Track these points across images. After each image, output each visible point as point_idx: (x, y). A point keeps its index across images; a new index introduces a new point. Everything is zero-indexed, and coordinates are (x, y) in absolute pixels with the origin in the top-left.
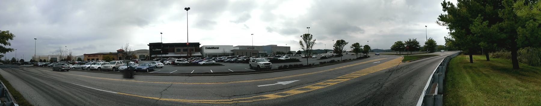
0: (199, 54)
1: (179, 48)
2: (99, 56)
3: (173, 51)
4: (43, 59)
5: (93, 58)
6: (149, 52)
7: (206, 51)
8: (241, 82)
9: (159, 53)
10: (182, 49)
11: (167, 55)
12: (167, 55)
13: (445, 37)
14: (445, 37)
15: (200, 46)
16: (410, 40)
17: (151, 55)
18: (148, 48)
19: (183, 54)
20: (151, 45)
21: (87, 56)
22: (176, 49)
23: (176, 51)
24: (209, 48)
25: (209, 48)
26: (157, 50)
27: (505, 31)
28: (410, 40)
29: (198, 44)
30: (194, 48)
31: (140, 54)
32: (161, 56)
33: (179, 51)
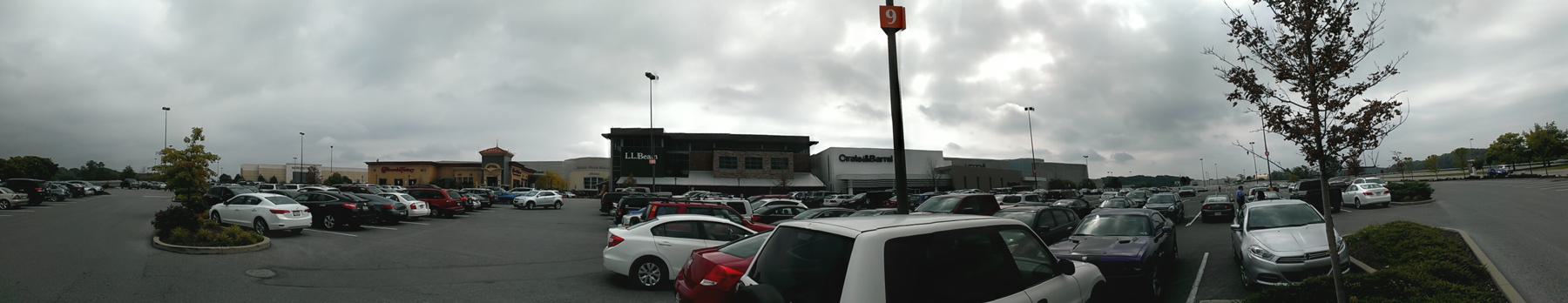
0: (813, 181)
1: (730, 153)
2: (417, 169)
3: (707, 167)
4: (267, 177)
5: (398, 175)
6: (609, 165)
7: (840, 170)
8: (1194, 290)
9: (644, 169)
10: (767, 156)
11: (682, 182)
12: (682, 182)
13: (197, 133)
14: (197, 133)
15: (814, 150)
16: (1537, 127)
17: (616, 175)
18: (604, 150)
19: (746, 177)
20: (618, 137)
21: (379, 169)
22: (717, 154)
23: (716, 164)
24: (856, 159)
25: (856, 159)
26: (640, 156)
27: (525, 175)
28: (1537, 127)
29: (805, 142)
30: (789, 155)
31: (586, 174)
32: (649, 181)
33: (728, 164)
